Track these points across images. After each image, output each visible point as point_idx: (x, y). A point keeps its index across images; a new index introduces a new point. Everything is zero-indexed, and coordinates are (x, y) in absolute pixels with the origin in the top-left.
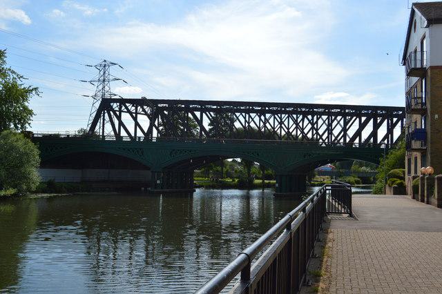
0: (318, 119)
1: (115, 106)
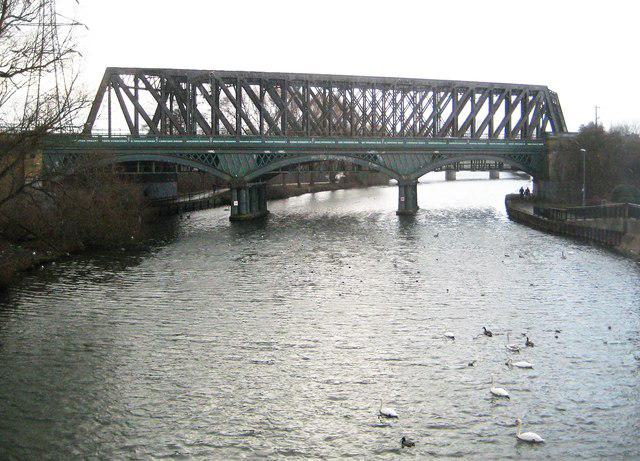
0: (403, 97)
1: (128, 80)
